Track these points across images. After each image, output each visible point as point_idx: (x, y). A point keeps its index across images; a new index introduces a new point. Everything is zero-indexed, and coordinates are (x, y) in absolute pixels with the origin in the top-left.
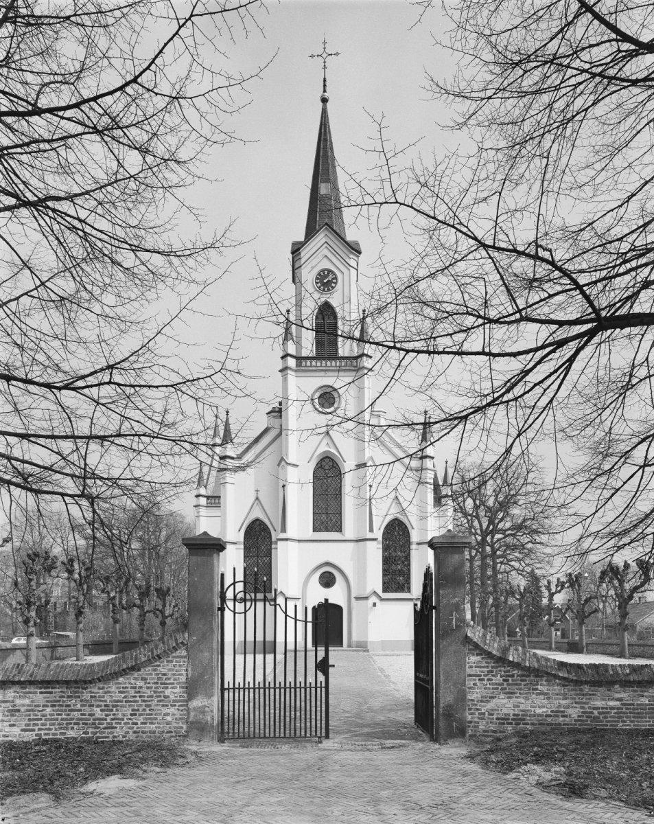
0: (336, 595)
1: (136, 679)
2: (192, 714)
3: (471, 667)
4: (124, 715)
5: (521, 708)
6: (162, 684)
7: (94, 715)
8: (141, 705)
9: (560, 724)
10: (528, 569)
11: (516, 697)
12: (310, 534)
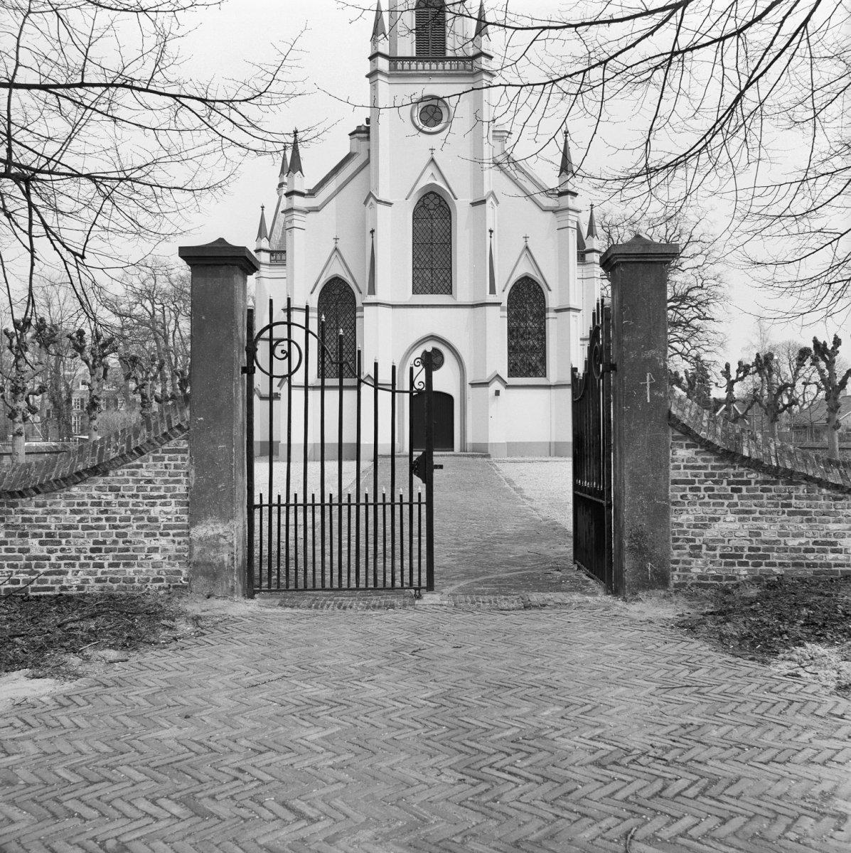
0: (445, 380)
1: (100, 489)
2: (197, 549)
3: (678, 468)
4: (80, 551)
5: (763, 537)
6: (144, 498)
7: (28, 550)
8: (109, 535)
9: (829, 565)
10: (694, 353)
11: (755, 519)
12: (407, 296)
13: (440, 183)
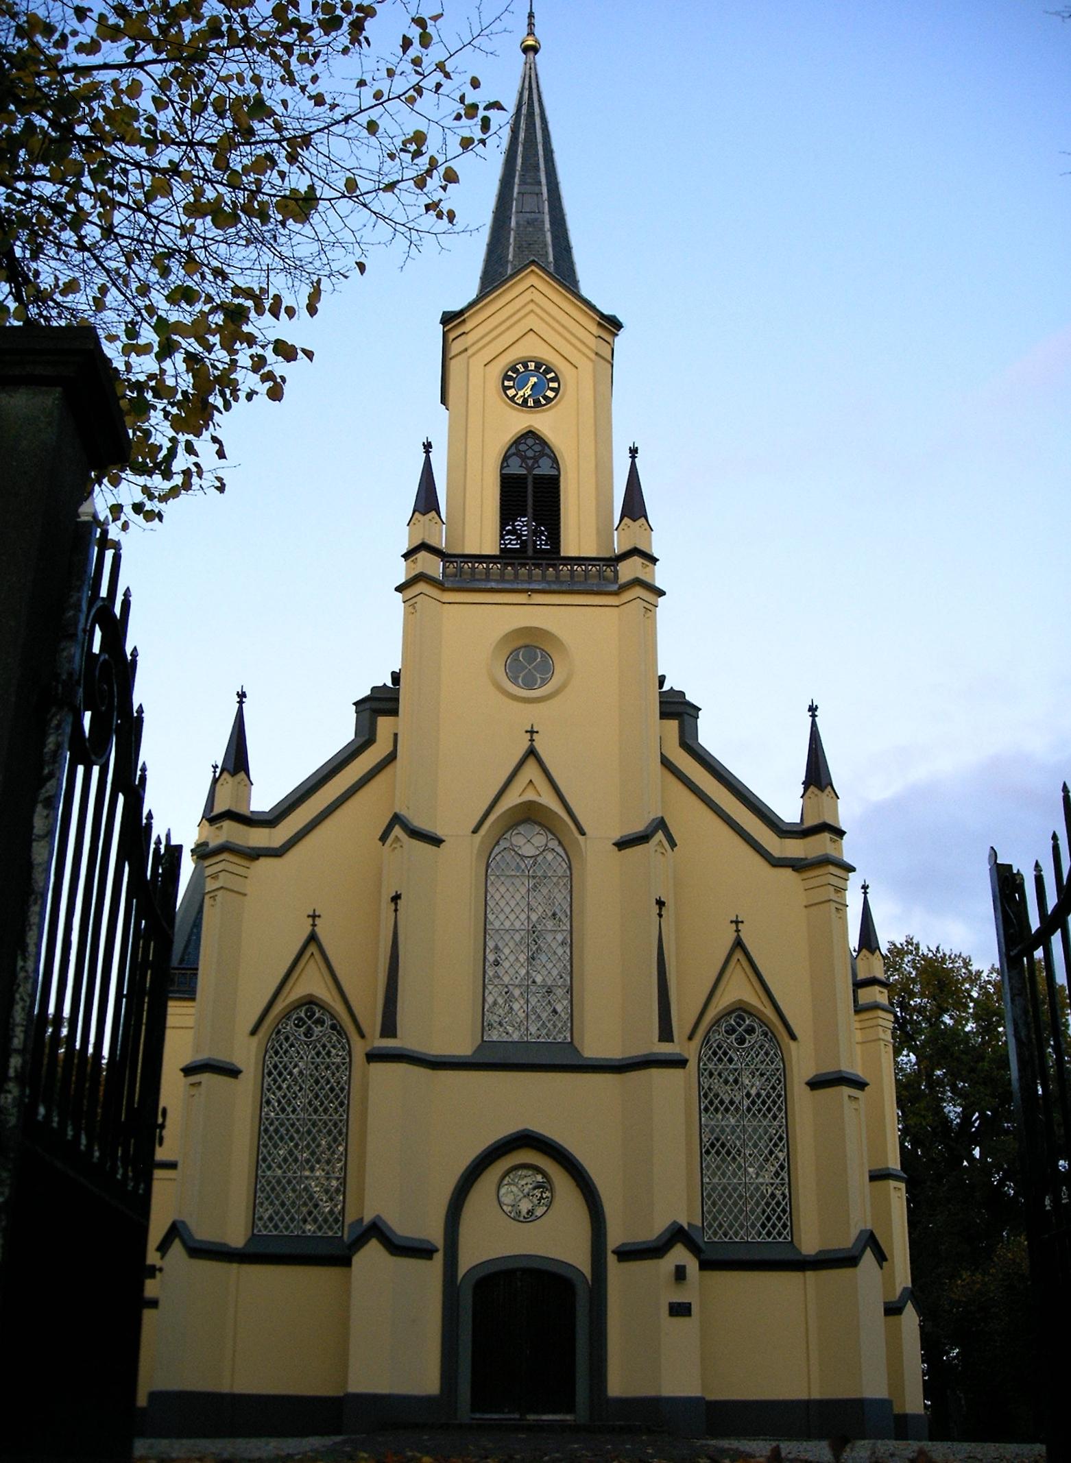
13: (548, 800)
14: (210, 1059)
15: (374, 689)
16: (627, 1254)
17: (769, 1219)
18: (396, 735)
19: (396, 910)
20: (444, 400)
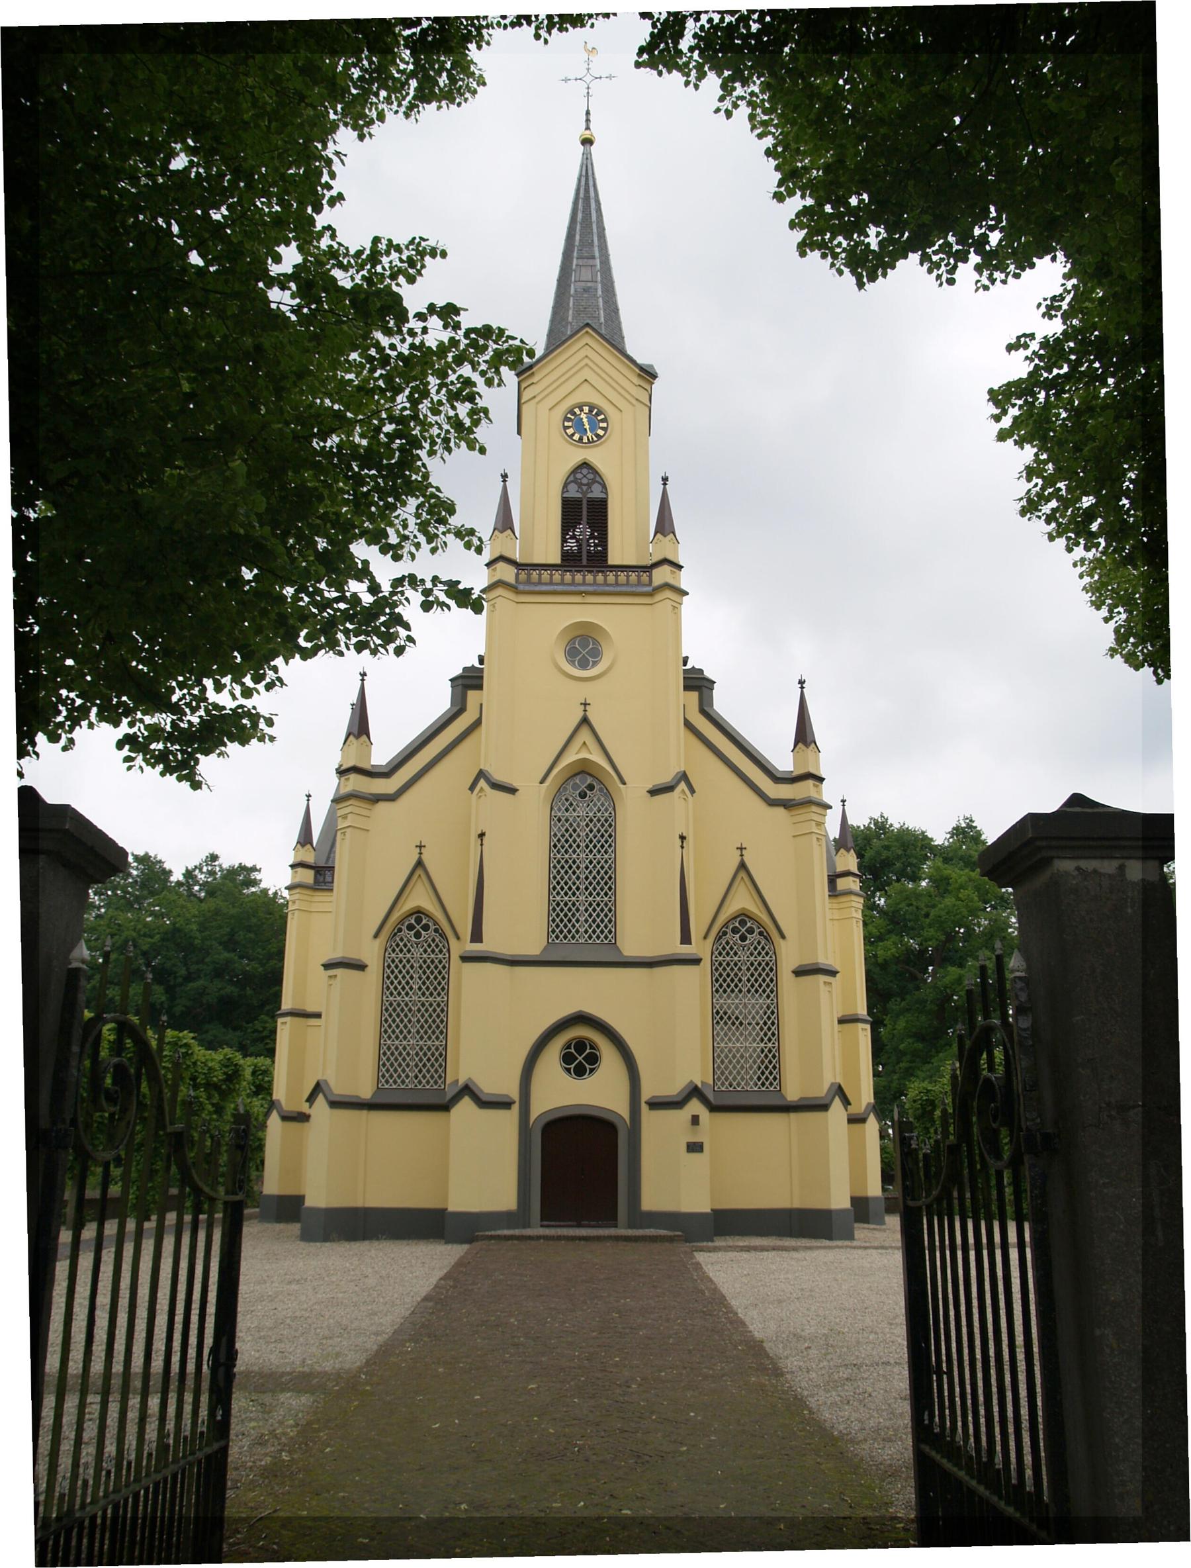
13: (597, 758)
14: (343, 957)
15: (465, 669)
16: (657, 1104)
17: (763, 1073)
18: (481, 705)
19: (482, 845)
20: (519, 433)
